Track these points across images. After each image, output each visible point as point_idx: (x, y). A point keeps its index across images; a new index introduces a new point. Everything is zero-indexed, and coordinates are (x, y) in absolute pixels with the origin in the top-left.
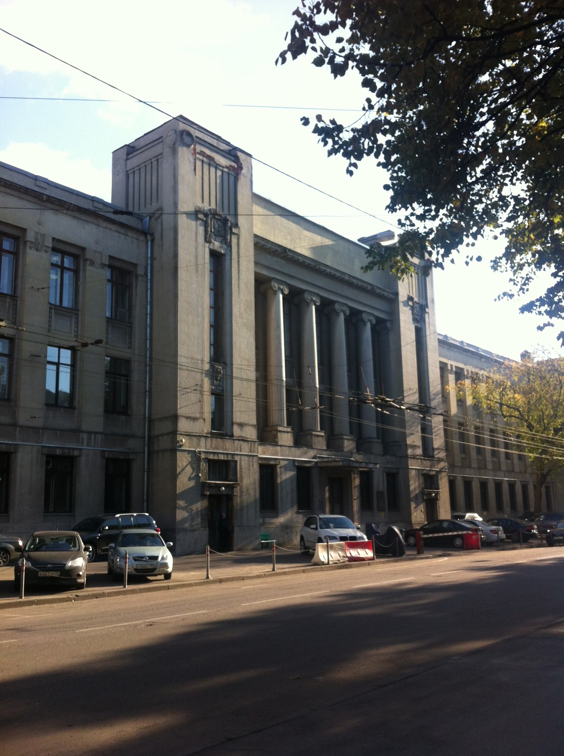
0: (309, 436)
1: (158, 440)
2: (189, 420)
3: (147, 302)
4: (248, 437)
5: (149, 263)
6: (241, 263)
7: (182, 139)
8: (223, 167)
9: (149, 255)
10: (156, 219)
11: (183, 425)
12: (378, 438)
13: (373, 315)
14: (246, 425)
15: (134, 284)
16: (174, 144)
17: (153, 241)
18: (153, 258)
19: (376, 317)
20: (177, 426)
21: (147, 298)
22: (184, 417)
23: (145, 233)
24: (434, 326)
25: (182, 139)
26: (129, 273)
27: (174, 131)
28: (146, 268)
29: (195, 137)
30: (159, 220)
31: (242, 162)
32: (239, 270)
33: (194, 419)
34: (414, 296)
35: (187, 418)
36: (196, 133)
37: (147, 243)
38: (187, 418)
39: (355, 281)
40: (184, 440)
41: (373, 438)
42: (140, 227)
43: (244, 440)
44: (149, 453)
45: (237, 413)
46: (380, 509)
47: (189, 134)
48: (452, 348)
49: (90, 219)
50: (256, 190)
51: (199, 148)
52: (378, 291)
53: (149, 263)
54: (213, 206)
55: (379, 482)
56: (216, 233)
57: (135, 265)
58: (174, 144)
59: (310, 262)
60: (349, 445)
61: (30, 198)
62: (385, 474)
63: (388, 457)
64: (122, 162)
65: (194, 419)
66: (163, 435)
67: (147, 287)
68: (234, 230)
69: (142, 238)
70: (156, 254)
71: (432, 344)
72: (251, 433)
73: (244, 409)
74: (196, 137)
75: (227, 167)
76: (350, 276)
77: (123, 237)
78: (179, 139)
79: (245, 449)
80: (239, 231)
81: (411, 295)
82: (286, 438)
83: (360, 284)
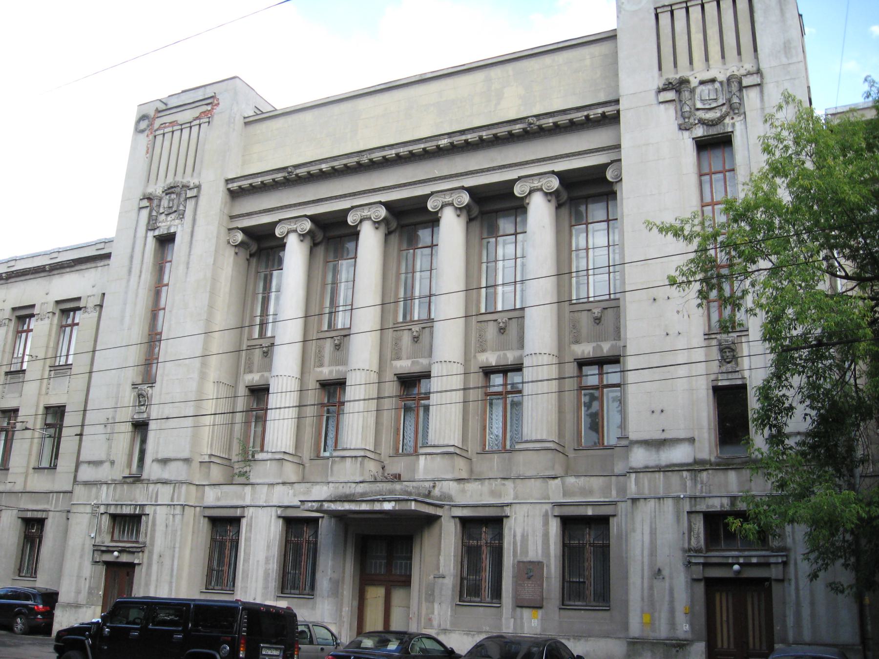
6: (195, 234)
49: (89, 265)
54: (170, 180)
61: (42, 274)
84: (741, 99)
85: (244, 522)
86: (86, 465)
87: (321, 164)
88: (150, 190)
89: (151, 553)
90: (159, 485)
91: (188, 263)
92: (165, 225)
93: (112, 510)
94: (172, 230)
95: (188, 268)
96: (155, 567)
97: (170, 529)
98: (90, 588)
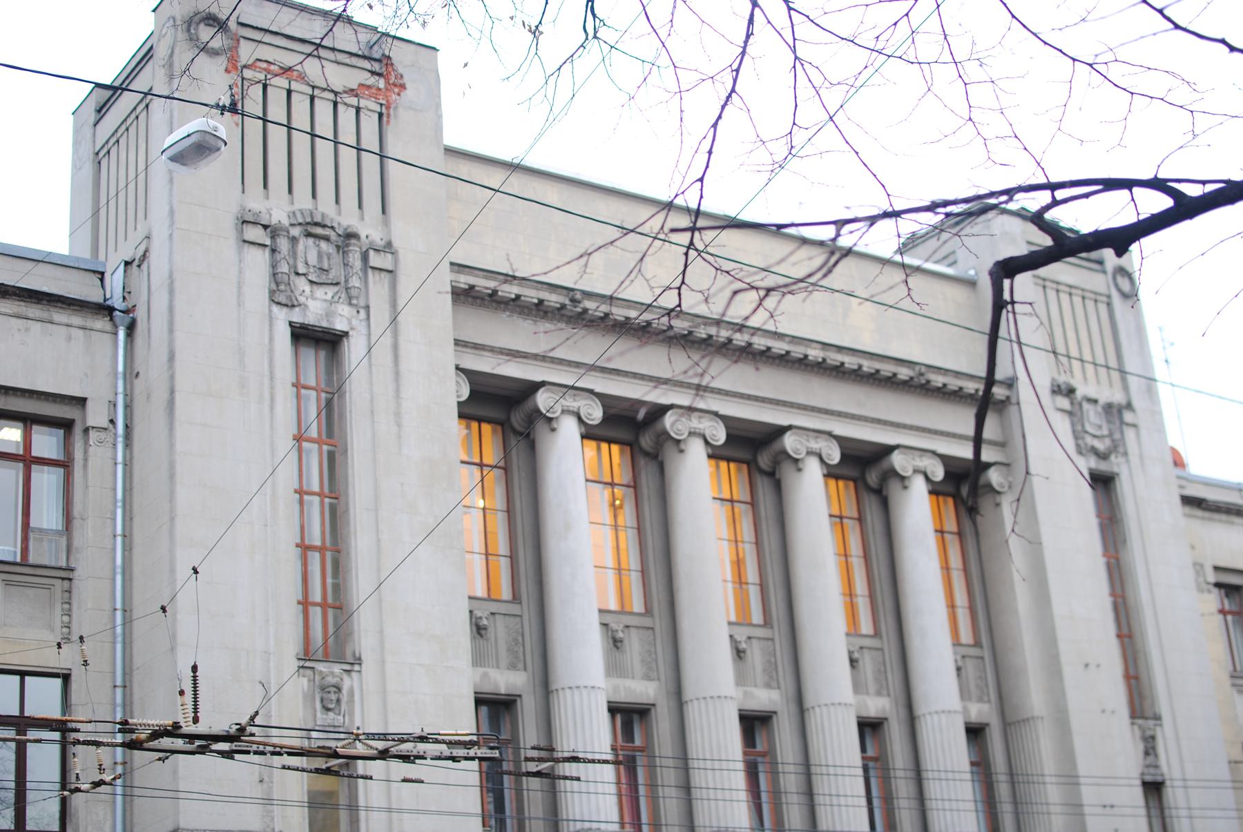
3: (116, 501)
6: (402, 353)
9: (121, 368)
10: (139, 266)
19: (945, 459)
21: (115, 489)
23: (105, 310)
25: (193, 39)
31: (401, 70)
32: (397, 374)
37: (116, 334)
42: (95, 296)
45: (375, 815)
53: (120, 389)
54: (303, 200)
56: (312, 277)
57: (81, 401)
64: (88, 131)
67: (115, 458)
69: (101, 323)
70: (139, 366)
75: (351, 92)
76: (825, 346)
77: (37, 327)
78: (181, 35)
80: (396, 262)
84: (1122, 433)
87: (629, 308)
88: (256, 203)
91: (398, 415)
92: (316, 308)
94: (340, 326)
95: (399, 425)
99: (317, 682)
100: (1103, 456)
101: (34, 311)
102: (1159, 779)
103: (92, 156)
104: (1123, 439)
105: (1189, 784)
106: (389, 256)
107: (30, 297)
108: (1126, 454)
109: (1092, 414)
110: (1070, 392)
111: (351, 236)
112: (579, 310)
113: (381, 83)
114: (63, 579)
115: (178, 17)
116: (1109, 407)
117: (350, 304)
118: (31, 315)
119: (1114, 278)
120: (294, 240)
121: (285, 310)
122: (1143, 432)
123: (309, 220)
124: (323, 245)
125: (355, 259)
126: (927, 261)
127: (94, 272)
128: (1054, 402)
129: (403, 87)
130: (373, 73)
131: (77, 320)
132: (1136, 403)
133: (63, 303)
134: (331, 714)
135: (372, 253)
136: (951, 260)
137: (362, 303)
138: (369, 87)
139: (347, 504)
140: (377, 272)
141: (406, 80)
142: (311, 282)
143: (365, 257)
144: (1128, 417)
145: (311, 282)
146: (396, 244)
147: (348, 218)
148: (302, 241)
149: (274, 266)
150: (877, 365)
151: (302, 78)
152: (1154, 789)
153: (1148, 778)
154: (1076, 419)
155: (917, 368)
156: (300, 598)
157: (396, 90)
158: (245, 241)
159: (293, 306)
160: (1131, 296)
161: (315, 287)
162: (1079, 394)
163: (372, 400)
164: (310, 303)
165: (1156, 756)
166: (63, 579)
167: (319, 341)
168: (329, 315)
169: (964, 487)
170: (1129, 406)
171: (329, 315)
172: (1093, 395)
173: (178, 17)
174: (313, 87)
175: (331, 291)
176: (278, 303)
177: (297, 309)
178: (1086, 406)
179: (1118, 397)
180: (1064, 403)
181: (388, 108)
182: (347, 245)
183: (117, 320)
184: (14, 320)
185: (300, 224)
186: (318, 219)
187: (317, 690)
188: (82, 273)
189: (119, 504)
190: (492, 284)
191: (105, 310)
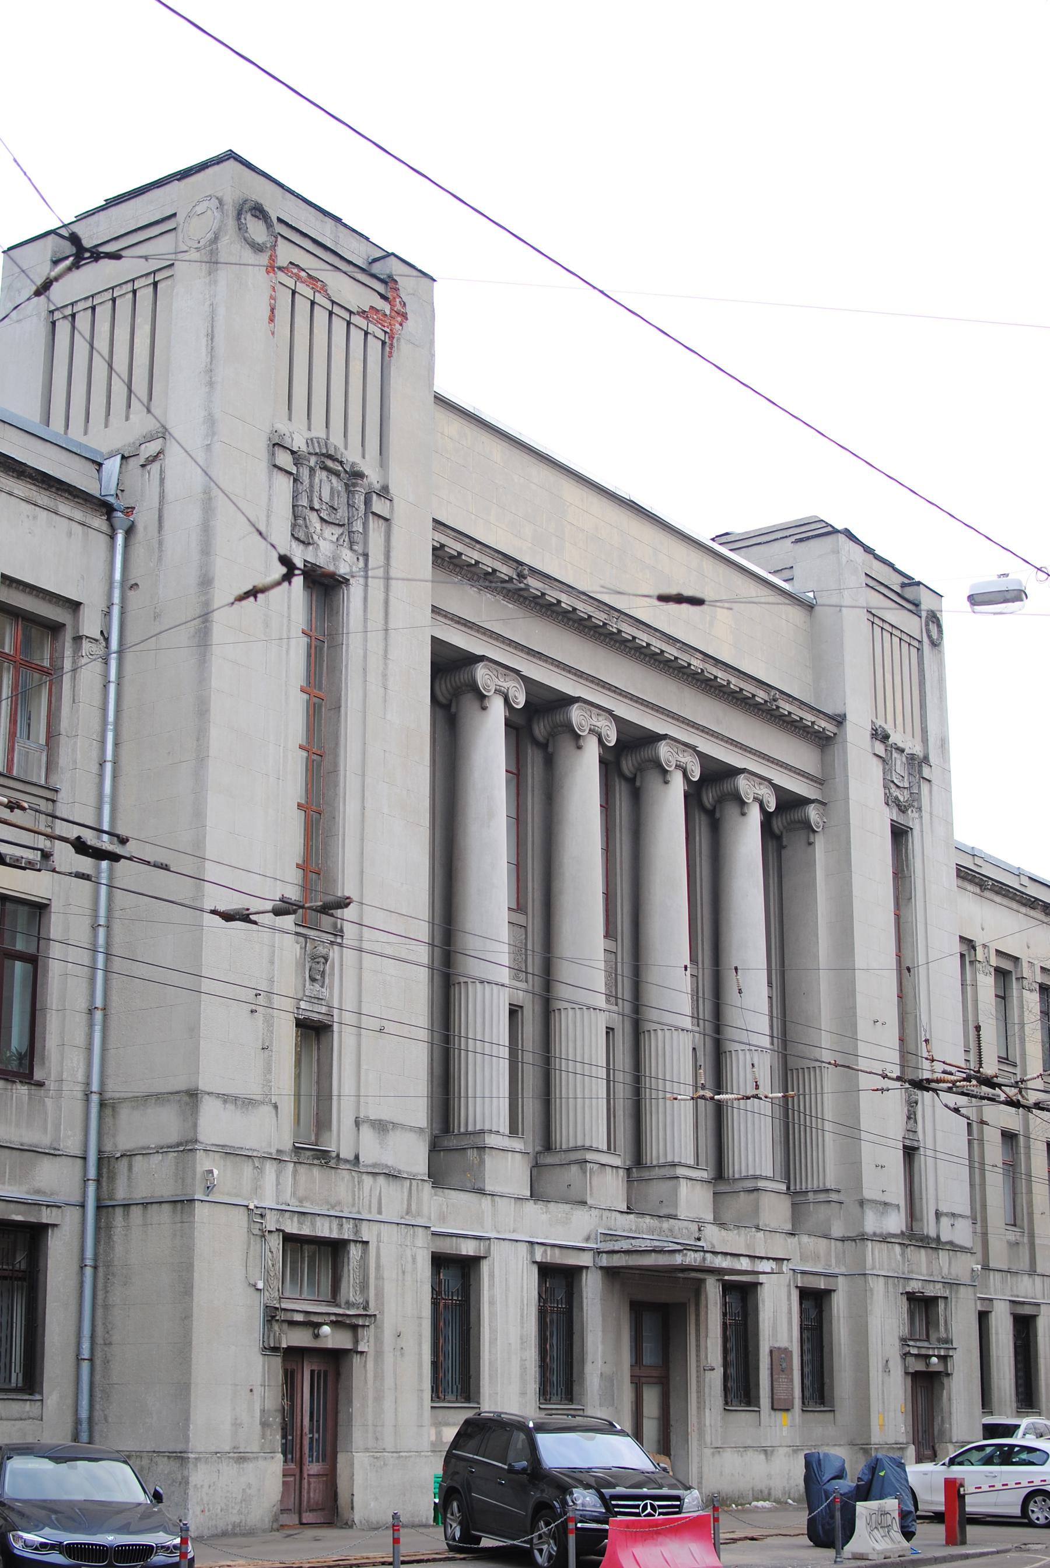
0: (472, 1154)
1: (130, 1168)
2: (230, 1107)
4: (401, 1168)
5: (116, 599)
7: (241, 228)
8: (351, 313)
9: (118, 576)
11: (216, 1124)
12: (610, 1149)
13: (694, 748)
14: (395, 1125)
15: (67, 665)
16: (216, 239)
17: (130, 532)
18: (129, 586)
20: (195, 1126)
22: (218, 1095)
23: (107, 509)
24: (949, 824)
25: (241, 228)
26: (55, 629)
27: (214, 203)
28: (108, 614)
29: (275, 221)
30: (155, 468)
33: (246, 1103)
34: (889, 728)
35: (226, 1098)
36: (277, 207)
37: (112, 537)
38: (226, 1098)
39: (720, 674)
40: (216, 1172)
41: (766, 1178)
42: (90, 487)
43: (393, 1176)
44: (99, 1208)
46: (779, 1406)
47: (259, 212)
48: (987, 894)
50: (445, 385)
51: (286, 253)
52: (786, 707)
53: (116, 599)
55: (778, 1321)
56: (323, 515)
57: (75, 606)
58: (216, 239)
59: (590, 610)
60: (693, 1199)
62: (795, 1295)
63: (805, 1239)
65: (246, 1103)
66: (145, 1153)
67: (106, 675)
68: (378, 506)
69: (99, 522)
71: (934, 873)
72: (411, 1154)
73: (384, 1077)
74: (279, 220)
75: (362, 313)
77: (43, 515)
78: (231, 223)
79: (393, 1200)
81: (880, 722)
82: (507, 1169)
83: (736, 683)
84: (919, 786)
85: (485, 1266)
86: (218, 1103)
89: (380, 1328)
90: (381, 1180)
91: (385, 676)
92: (327, 551)
93: (292, 1227)
94: (343, 570)
96: (389, 1358)
97: (408, 1277)
98: (263, 1411)
99: (308, 952)
100: (902, 809)
101: (43, 498)
102: (916, 1144)
103: (44, 314)
104: (919, 794)
105: (939, 1155)
106: (388, 502)
107: (43, 482)
108: (920, 809)
109: (898, 762)
110: (886, 737)
111: (359, 475)
112: (522, 585)
113: (386, 308)
114: (48, 799)
115: (228, 200)
116: (912, 757)
117: (351, 549)
118: (40, 502)
119: (927, 625)
120: (312, 470)
121: (301, 546)
122: (935, 788)
123: (324, 451)
124: (334, 479)
125: (359, 500)
126: (775, 572)
127: (94, 462)
128: (873, 747)
129: (404, 316)
130: (383, 297)
131: (78, 514)
132: (932, 759)
133: (70, 493)
134: (317, 986)
135: (375, 496)
136: (787, 574)
137: (360, 551)
138: (377, 311)
139: (336, 765)
140: (376, 518)
141: (408, 309)
142: (322, 519)
143: (367, 502)
144: (926, 772)
145: (322, 519)
146: (393, 490)
147: (352, 456)
148: (318, 472)
149: (295, 497)
150: (742, 685)
151: (323, 289)
152: (910, 1153)
153: (908, 1143)
154: (887, 767)
155: (773, 692)
156: (300, 862)
157: (399, 319)
158: (275, 466)
159: (309, 544)
160: (936, 644)
161: (325, 526)
162: (891, 740)
163: (365, 657)
164: (321, 543)
165: (916, 1122)
166: (48, 799)
167: (324, 586)
168: (335, 558)
169: (787, 824)
170: (926, 759)
171: (335, 558)
172: (901, 745)
173: (228, 200)
174: (333, 302)
175: (338, 531)
176: (297, 539)
177: (311, 547)
178: (895, 755)
179: (918, 750)
180: (880, 748)
181: (391, 338)
182: (354, 485)
183: (117, 523)
184: (23, 504)
185: (316, 454)
186: (332, 452)
187: (308, 959)
188: (83, 460)
189: (110, 727)
190: (459, 547)
191: (107, 509)
